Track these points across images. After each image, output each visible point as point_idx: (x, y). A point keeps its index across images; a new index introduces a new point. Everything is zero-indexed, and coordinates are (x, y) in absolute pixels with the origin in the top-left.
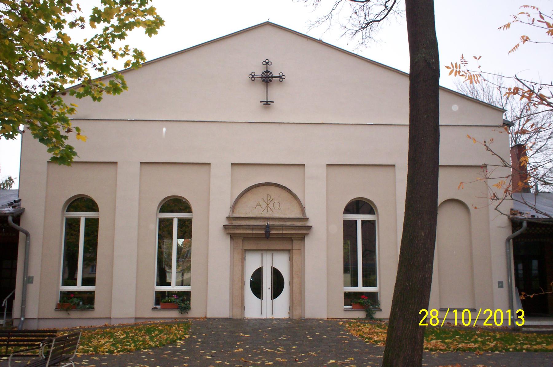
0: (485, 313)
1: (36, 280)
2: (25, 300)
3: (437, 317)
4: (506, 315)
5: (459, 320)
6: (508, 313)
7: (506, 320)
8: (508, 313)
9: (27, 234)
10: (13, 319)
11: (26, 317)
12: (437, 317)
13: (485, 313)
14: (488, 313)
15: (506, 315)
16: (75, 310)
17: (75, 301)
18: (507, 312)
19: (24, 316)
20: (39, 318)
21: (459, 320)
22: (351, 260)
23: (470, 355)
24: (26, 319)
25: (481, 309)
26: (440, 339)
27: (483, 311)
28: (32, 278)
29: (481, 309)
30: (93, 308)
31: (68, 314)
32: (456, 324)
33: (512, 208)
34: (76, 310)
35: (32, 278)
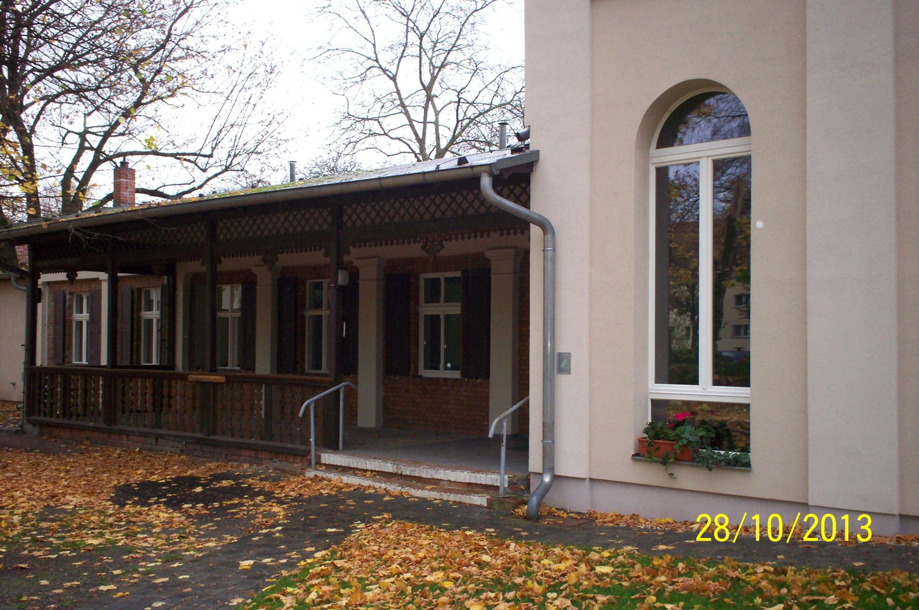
0: (805, 520)
1: (579, 363)
2: (553, 423)
3: (869, 527)
4: (841, 524)
5: (763, 528)
6: (844, 520)
7: (840, 534)
8: (844, 520)
9: (545, 226)
10: (529, 475)
11: (557, 473)
12: (869, 527)
13: (805, 520)
14: (811, 520)
15: (841, 524)
16: (687, 465)
17: (687, 435)
18: (843, 518)
19: (552, 469)
20: (592, 480)
21: (763, 528)
22: (315, 416)
23: (149, 569)
24: (555, 477)
25: (746, 514)
26: (118, 546)
27: (802, 517)
28: (568, 356)
29: (746, 514)
30: (748, 465)
31: (671, 475)
32: (758, 539)
33: (16, 384)
34: (693, 465)
35: (568, 356)
